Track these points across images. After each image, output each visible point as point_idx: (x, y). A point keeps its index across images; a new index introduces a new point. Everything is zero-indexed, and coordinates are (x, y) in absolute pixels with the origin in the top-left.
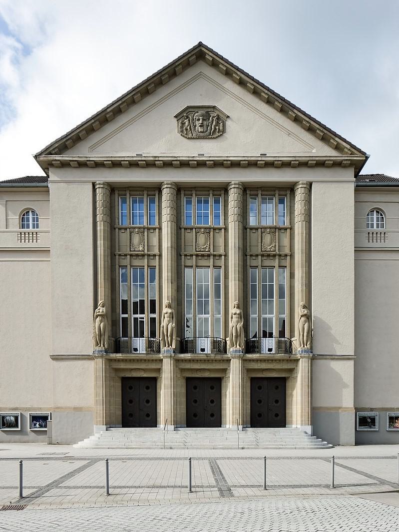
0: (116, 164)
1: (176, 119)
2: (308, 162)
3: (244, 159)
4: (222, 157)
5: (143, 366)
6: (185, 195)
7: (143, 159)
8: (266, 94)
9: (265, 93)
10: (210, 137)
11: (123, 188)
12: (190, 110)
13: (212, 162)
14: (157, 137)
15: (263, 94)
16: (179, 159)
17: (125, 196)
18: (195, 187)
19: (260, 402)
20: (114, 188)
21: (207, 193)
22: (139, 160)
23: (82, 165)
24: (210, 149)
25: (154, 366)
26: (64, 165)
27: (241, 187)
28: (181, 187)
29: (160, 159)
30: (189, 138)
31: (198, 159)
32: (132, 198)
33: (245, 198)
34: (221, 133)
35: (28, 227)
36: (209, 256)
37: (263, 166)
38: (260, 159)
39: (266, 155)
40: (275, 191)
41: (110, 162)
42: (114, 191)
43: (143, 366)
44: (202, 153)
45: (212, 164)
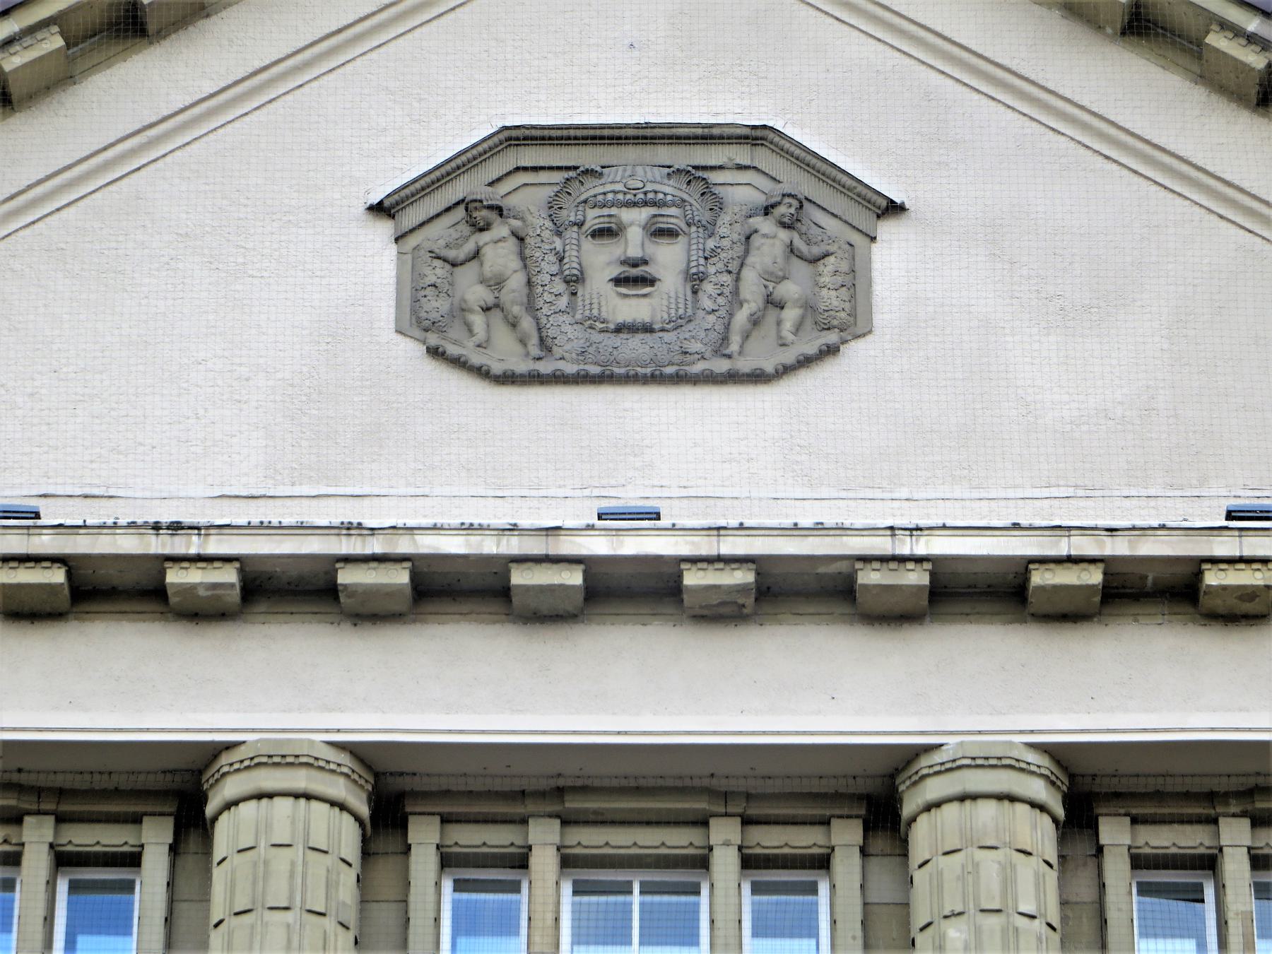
1: (384, 229)
2: (1026, 574)
3: (1063, 547)
4: (841, 529)
6: (447, 861)
7: (45, 544)
8: (1251, 39)
9: (1237, 32)
10: (722, 366)
11: (1188, 796)
12: (530, 156)
13: (743, 577)
15: (1218, 40)
16: (404, 546)
17: (692, 899)
18: (560, 792)
20: (401, 797)
21: (679, 840)
22: (694, 560)
24: (710, 466)
27: (1038, 789)
28: (407, 784)
29: (215, 546)
30: (508, 379)
31: (598, 546)
32: (74, 887)
33: (1083, 890)
34: (832, 337)
37: (402, 605)
38: (1224, 547)
39: (657, 516)
40: (703, 822)
41: (57, 576)
42: (403, 827)
44: (631, 497)
45: (742, 589)
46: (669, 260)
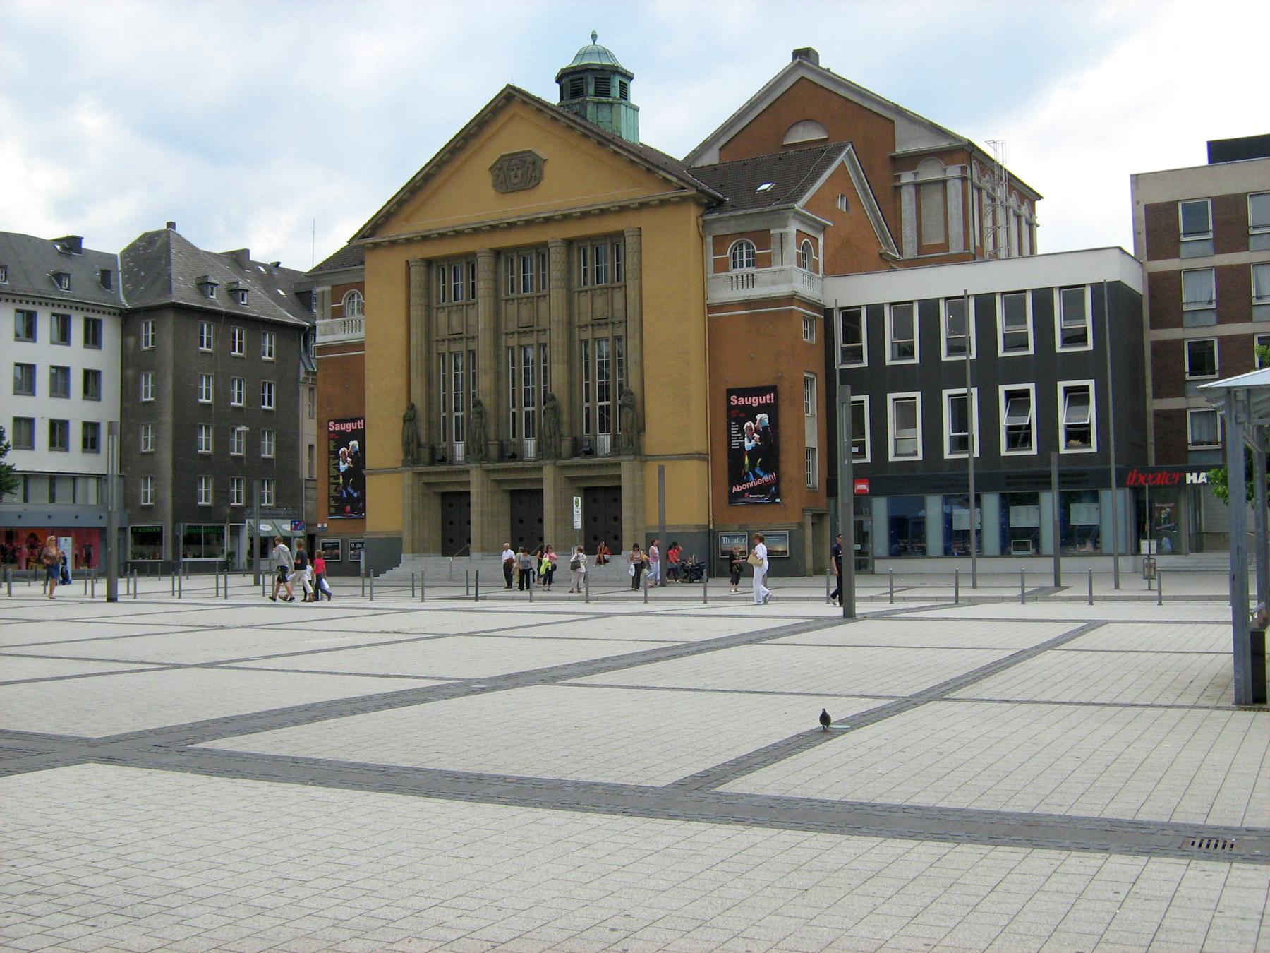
0: (425, 238)
5: (454, 479)
14: (473, 201)
19: (521, 521)
23: (393, 243)
25: (535, 476)
26: (376, 246)
35: (741, 266)
36: (607, 324)
43: (603, 472)
46: (520, 172)
